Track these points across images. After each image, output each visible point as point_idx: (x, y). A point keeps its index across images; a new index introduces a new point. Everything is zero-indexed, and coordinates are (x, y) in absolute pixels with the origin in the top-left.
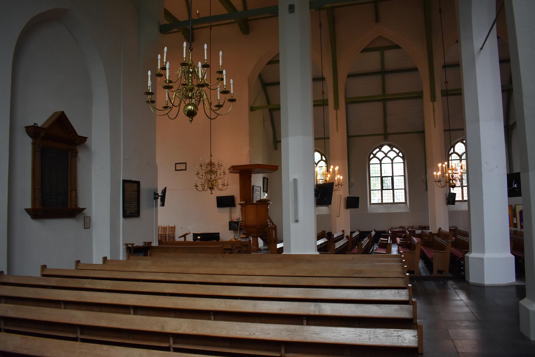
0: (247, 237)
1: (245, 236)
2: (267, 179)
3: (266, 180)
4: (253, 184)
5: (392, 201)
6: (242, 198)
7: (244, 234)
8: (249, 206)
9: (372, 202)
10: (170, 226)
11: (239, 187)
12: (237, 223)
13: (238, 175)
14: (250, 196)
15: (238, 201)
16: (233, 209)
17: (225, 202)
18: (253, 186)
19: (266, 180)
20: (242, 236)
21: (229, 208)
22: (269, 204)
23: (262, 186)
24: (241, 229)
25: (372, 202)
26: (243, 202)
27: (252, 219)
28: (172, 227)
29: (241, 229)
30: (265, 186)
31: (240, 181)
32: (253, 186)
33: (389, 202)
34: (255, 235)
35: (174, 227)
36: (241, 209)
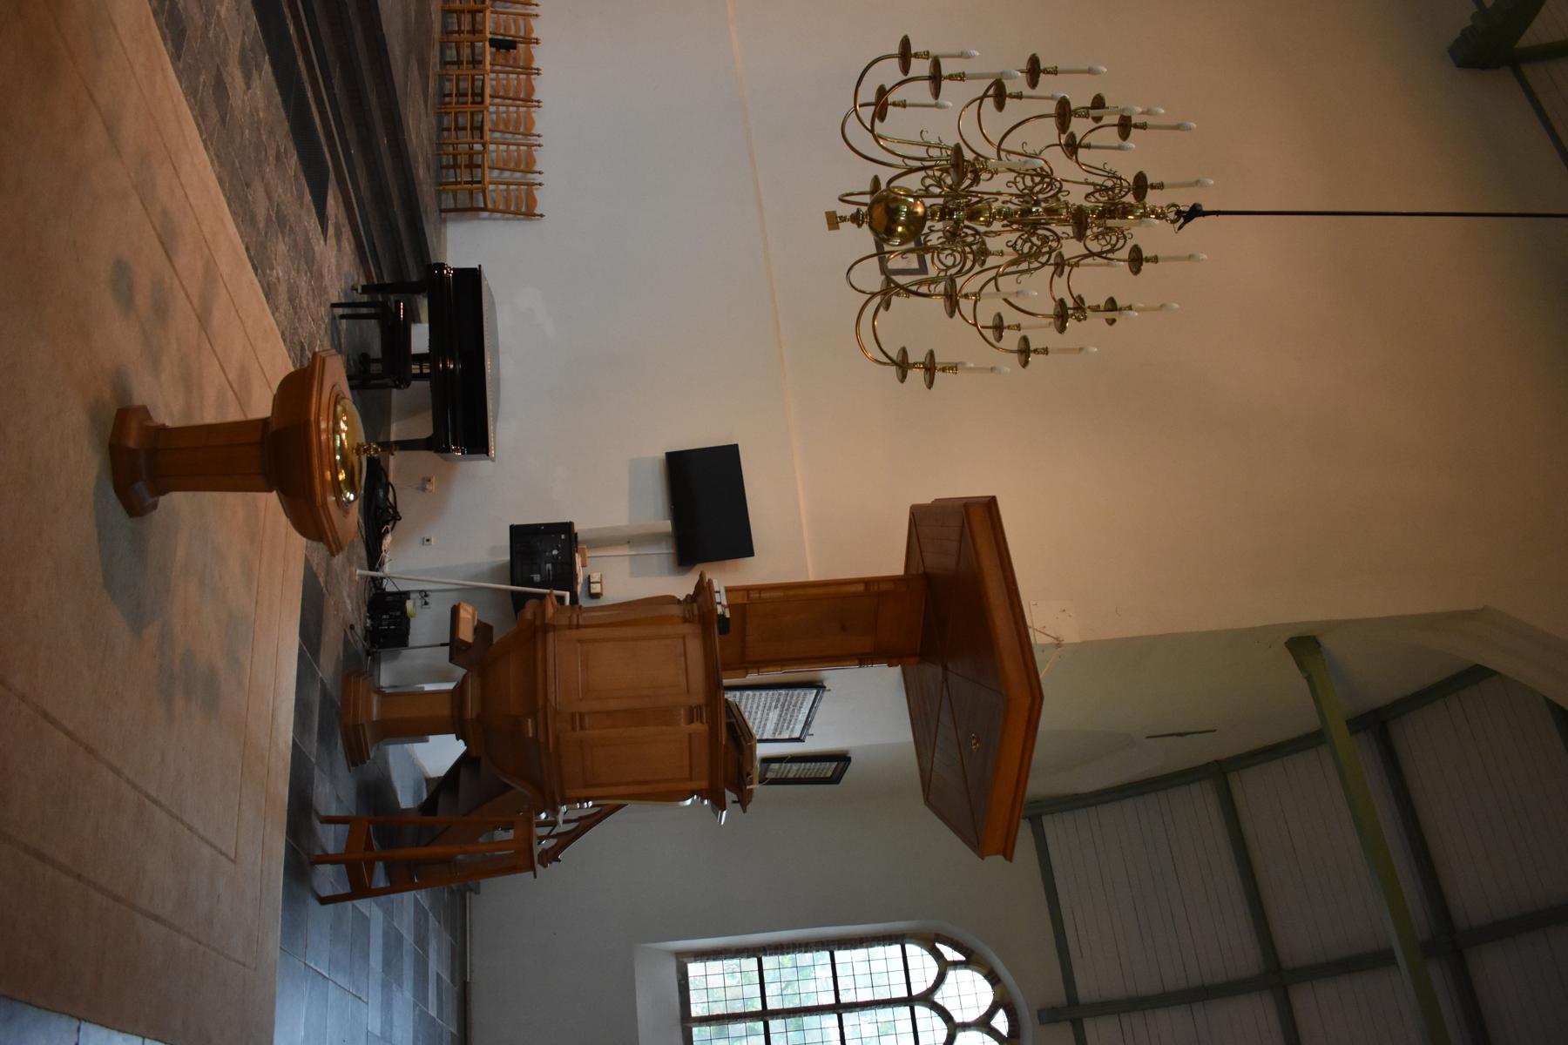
0: (457, 649)
1: (466, 634)
2: (835, 779)
3: (828, 769)
4: (833, 677)
5: (697, 1010)
6: (749, 600)
7: (482, 630)
8: (695, 648)
9: (695, 969)
10: (539, 194)
11: (812, 577)
12: (565, 577)
13: (897, 567)
14: (758, 665)
15: (725, 578)
16: (665, 551)
17: (704, 499)
18: (818, 686)
19: (828, 769)
20: (466, 614)
21: (667, 526)
22: (719, 804)
23: (809, 746)
24: (519, 601)
25: (695, 969)
26: (721, 598)
27: (583, 674)
28: (531, 201)
29: (519, 601)
30: (794, 770)
31: (867, 582)
32: (818, 686)
33: (694, 996)
34: (471, 710)
35: (530, 214)
36: (671, 600)
